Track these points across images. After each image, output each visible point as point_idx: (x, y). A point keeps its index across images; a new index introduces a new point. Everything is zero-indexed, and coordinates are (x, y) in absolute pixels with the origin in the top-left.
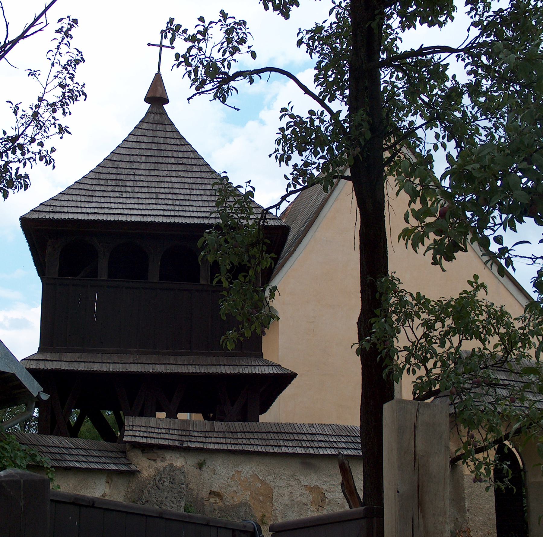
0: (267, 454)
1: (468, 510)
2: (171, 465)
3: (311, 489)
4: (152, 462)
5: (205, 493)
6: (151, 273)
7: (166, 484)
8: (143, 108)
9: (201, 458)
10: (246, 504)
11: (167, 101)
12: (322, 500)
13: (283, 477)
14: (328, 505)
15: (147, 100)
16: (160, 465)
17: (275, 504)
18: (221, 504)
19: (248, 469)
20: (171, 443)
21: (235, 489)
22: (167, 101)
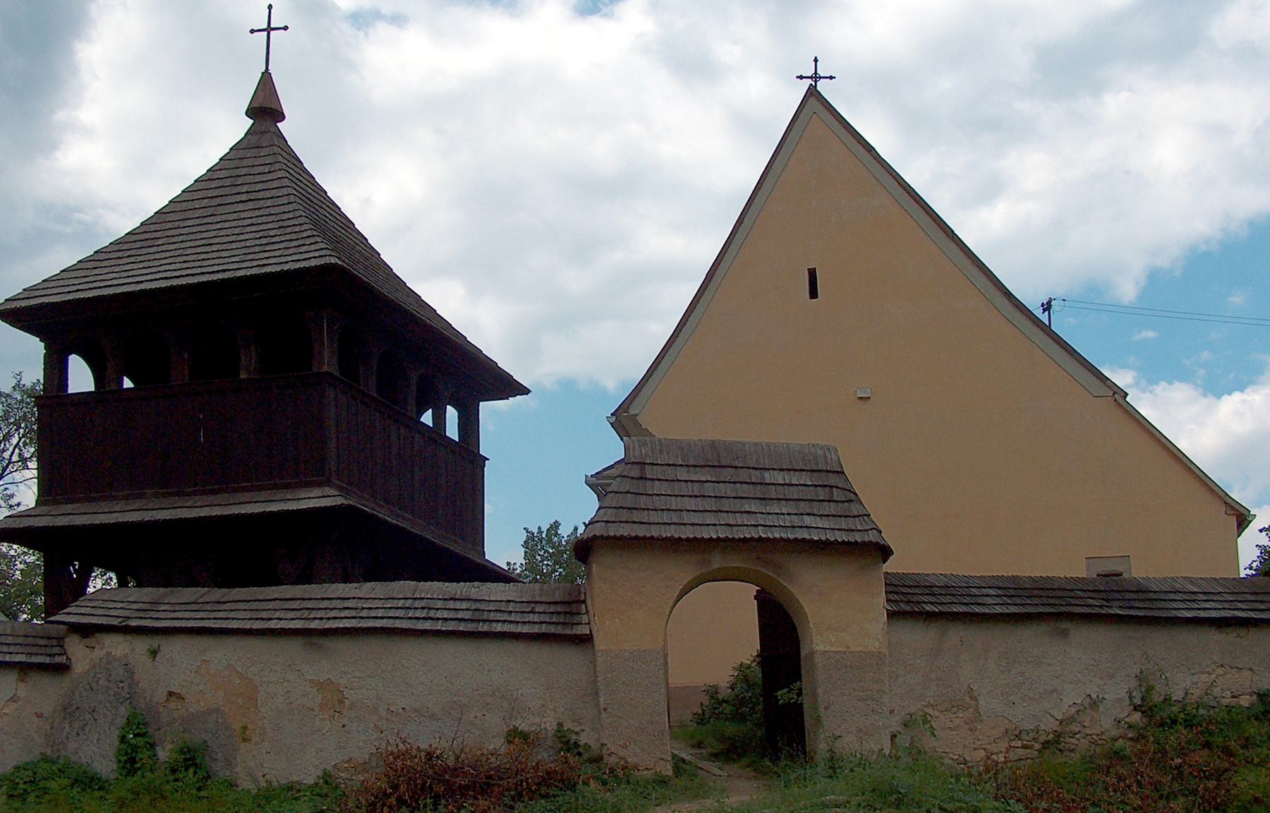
0: (424, 633)
1: (605, 709)
2: (109, 653)
3: (320, 686)
4: (88, 651)
5: (161, 696)
6: (263, 374)
7: (101, 682)
8: (237, 127)
9: (154, 642)
10: (217, 711)
11: (282, 117)
12: (341, 702)
13: (274, 668)
14: (350, 709)
15: (250, 113)
16: (99, 653)
17: (262, 710)
18: (182, 711)
19: (221, 654)
20: (115, 622)
21: (201, 688)
22: (282, 117)
